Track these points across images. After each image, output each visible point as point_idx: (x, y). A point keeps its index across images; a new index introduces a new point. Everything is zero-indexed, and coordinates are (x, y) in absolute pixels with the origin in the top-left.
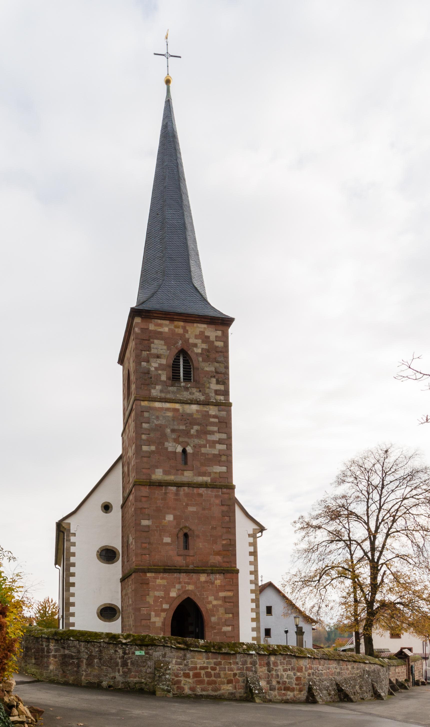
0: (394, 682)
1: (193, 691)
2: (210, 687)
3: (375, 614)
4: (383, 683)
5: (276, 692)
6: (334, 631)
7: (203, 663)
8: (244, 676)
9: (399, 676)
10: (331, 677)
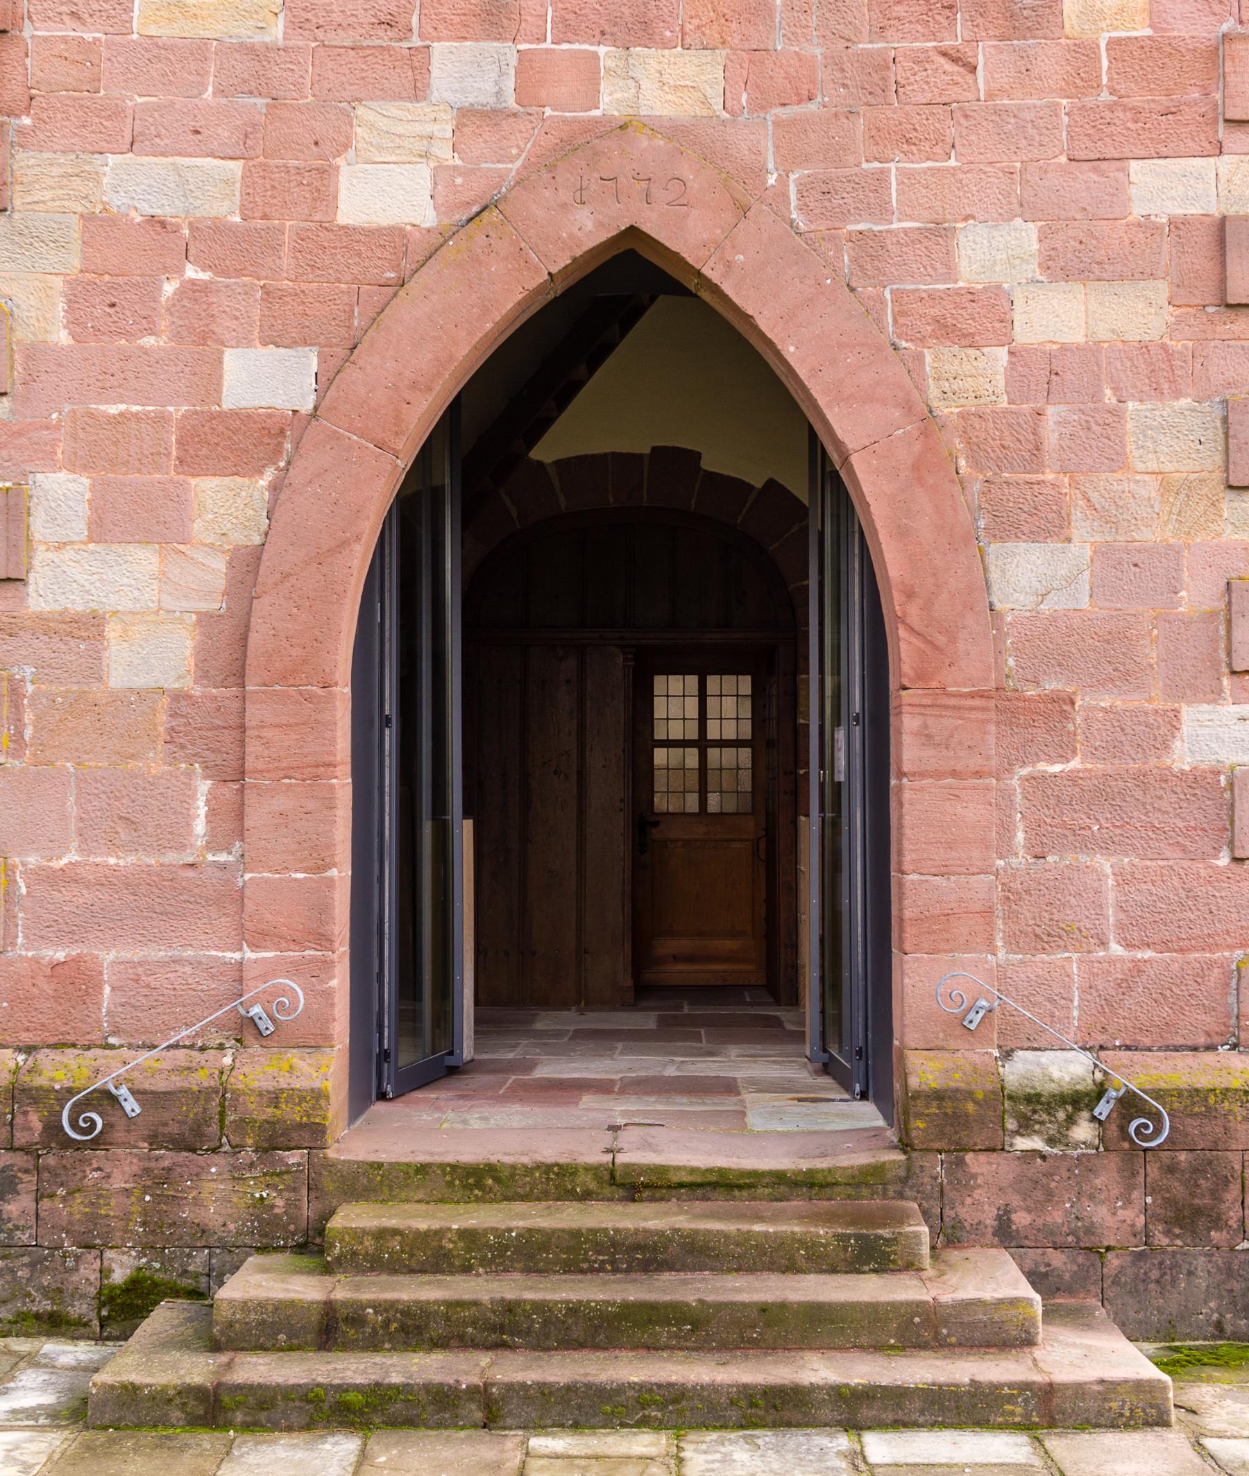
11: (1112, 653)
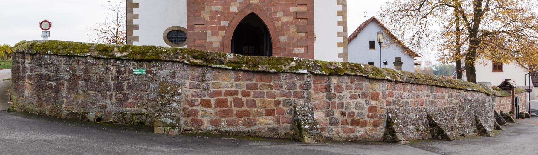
0: (499, 114)
1: (215, 126)
2: (241, 120)
3: (479, 42)
4: (489, 115)
5: (340, 128)
6: (440, 70)
7: (230, 86)
8: (291, 105)
9: (504, 108)
10: (421, 107)
11: (288, 44)
